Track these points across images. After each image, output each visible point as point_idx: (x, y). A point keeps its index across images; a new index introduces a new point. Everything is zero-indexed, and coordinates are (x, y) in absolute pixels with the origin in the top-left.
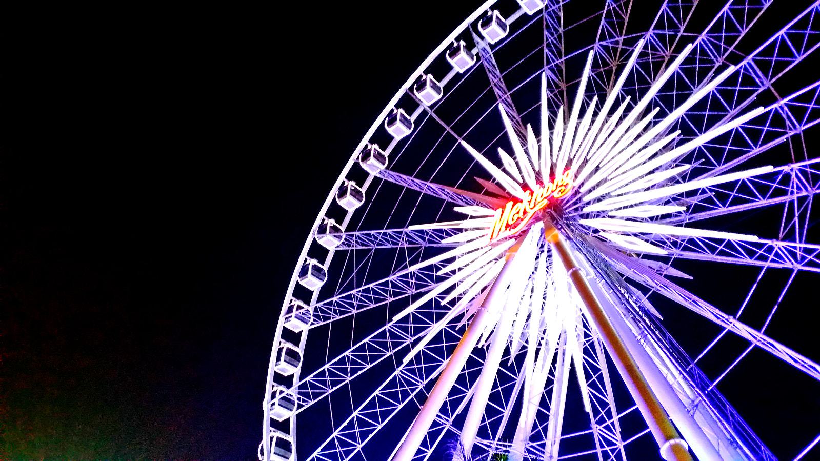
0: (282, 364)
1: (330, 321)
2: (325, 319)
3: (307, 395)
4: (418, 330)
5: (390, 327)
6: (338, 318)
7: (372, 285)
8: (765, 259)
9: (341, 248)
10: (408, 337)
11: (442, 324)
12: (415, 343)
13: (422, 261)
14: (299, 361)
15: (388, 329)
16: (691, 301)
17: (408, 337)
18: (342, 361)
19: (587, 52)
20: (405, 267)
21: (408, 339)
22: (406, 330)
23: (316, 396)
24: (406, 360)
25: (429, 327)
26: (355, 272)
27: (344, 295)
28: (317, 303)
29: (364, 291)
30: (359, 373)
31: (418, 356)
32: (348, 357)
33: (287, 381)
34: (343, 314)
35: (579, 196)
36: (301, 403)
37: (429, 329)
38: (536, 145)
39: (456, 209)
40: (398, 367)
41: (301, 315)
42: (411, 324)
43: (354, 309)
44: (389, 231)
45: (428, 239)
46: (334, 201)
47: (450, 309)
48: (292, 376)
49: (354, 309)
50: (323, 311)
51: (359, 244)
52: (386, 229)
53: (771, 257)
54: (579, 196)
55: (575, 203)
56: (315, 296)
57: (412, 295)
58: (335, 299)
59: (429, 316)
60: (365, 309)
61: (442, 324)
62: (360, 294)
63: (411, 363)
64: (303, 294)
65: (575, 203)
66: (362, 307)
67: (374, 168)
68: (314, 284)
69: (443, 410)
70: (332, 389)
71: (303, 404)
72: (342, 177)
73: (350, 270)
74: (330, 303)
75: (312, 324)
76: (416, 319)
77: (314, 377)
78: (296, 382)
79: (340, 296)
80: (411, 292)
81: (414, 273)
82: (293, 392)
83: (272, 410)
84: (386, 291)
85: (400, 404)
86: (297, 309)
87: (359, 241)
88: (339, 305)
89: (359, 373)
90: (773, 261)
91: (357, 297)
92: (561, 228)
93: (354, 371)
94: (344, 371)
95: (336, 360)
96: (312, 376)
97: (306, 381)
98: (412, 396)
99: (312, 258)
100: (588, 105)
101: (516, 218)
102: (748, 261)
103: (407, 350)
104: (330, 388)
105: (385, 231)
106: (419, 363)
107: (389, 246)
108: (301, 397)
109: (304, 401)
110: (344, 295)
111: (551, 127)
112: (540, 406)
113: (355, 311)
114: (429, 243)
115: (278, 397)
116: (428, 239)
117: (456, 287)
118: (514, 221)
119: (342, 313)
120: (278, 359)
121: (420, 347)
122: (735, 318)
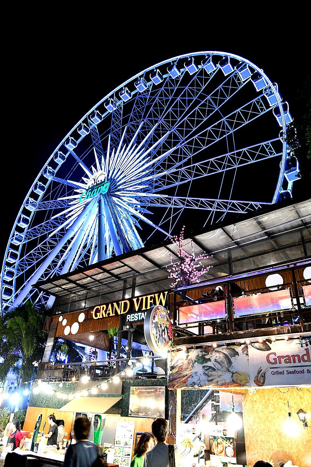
1: (48, 253)
10: (183, 171)
11: (165, 173)
12: (180, 167)
13: (148, 133)
19: (125, 126)
24: (186, 160)
25: (170, 173)
26: (172, 216)
30: (219, 157)
31: (181, 160)
35: (116, 186)
38: (90, 232)
42: (226, 162)
54: (116, 186)
55: (115, 186)
61: (165, 173)
63: (185, 158)
65: (115, 186)
73: (174, 219)
77: (248, 162)
84: (46, 247)
92: (187, 325)
98: (235, 152)
100: (123, 146)
103: (185, 164)
104: (227, 156)
106: (181, 157)
111: (100, 164)
121: (178, 164)
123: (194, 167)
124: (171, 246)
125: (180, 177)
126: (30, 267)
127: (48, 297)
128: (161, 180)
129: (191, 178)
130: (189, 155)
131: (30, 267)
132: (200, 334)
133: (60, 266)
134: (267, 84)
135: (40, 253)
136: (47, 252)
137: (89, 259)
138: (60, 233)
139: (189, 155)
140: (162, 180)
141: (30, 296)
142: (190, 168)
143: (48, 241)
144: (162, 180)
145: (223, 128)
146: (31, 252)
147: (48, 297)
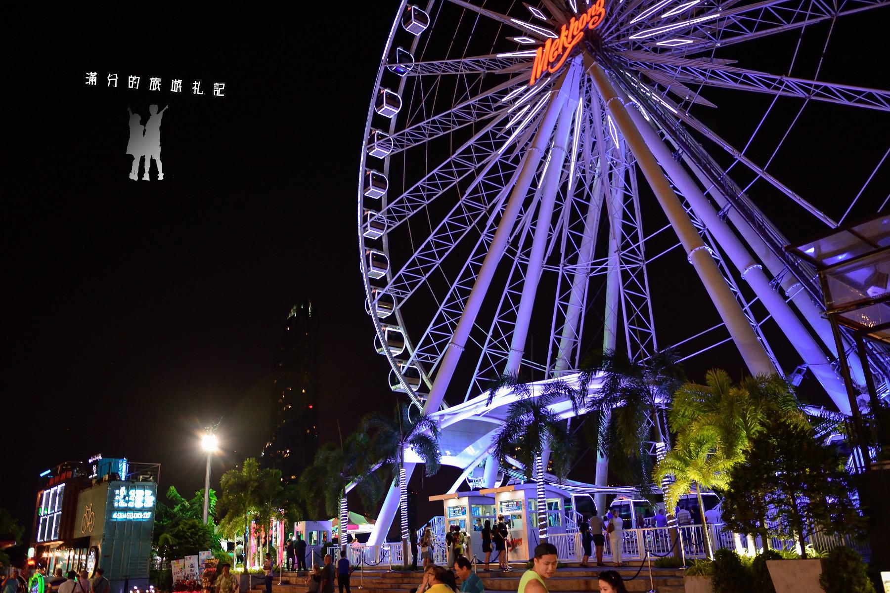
0: (373, 270)
1: (406, 218)
2: (400, 218)
4: (491, 197)
10: (482, 207)
15: (464, 204)
16: (741, 79)
17: (482, 207)
18: (428, 247)
21: (484, 209)
23: (412, 286)
27: (414, 127)
28: (388, 205)
29: (428, 179)
30: (446, 254)
32: (432, 240)
33: (382, 283)
40: (482, 232)
42: (482, 192)
43: (425, 200)
44: (436, 117)
45: (476, 113)
46: (375, 113)
47: (515, 168)
48: (385, 277)
49: (425, 200)
50: (396, 211)
52: (433, 117)
57: (476, 170)
58: (407, 130)
59: (498, 180)
60: (434, 197)
62: (426, 183)
64: (381, 122)
66: (433, 135)
67: (406, 70)
68: (391, 112)
70: (425, 275)
72: (377, 86)
75: (389, 227)
76: (487, 187)
77: (434, 325)
79: (411, 128)
80: (473, 120)
82: (389, 289)
83: (377, 312)
84: (403, 207)
85: (497, 321)
86: (378, 139)
91: (428, 129)
93: (441, 254)
94: (432, 256)
95: (423, 246)
96: (404, 268)
99: (377, 128)
105: (433, 119)
107: (442, 134)
110: (414, 127)
112: (623, 219)
113: (427, 140)
115: (377, 298)
116: (476, 113)
117: (523, 205)
118: (555, 58)
119: (414, 208)
122: (787, 76)
123: (471, 223)
124: (823, 378)
126: (415, 211)
127: (731, 338)
129: (464, 202)
130: (466, 201)
131: (415, 211)
133: (492, 226)
134: (368, 257)
135: (436, 186)
137: (393, 370)
139: (466, 201)
142: (475, 217)
146: (419, 184)
147: (731, 338)
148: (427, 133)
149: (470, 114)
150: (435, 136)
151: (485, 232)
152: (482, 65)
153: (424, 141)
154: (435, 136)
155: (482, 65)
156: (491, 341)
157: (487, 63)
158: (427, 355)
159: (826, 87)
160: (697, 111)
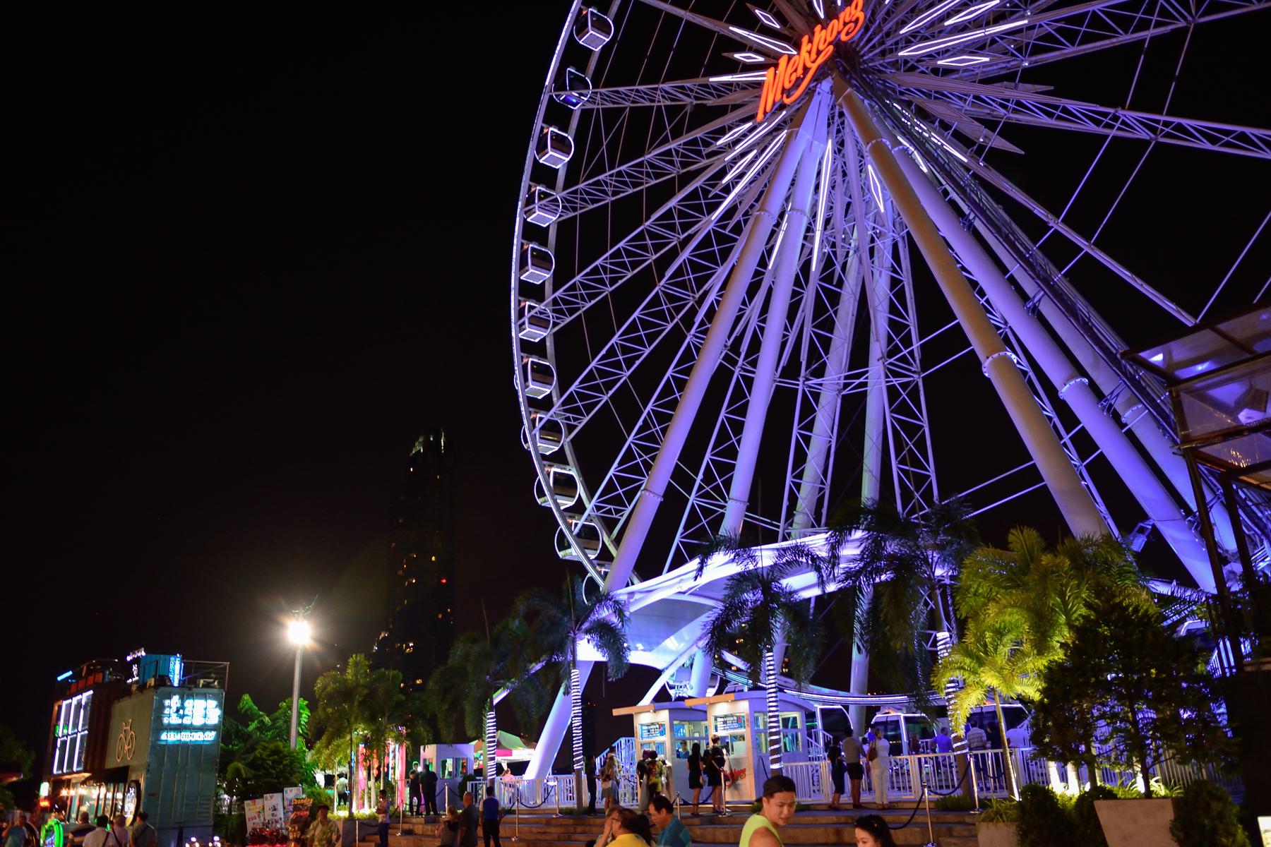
0: (532, 386)
2: (572, 312)
3: (576, 411)
4: (701, 282)
5: (663, 286)
6: (588, 305)
7: (621, 245)
8: (1111, 127)
9: (565, 217)
10: (689, 296)
13: (680, 189)
14: (553, 376)
15: (662, 291)
17: (689, 296)
18: (612, 352)
20: (665, 141)
22: (682, 285)
23: (589, 408)
27: (591, 181)
29: (612, 256)
30: (638, 363)
32: (617, 343)
33: (546, 404)
34: (594, 299)
36: (573, 423)
37: (716, 275)
39: (691, 753)
41: (539, 315)
45: (681, 162)
47: (736, 240)
50: (565, 302)
51: (587, 202)
53: (1118, 125)
56: (548, 288)
57: (680, 242)
58: (581, 186)
59: (711, 257)
62: (614, 178)
66: (618, 193)
69: (749, 382)
70: (607, 393)
71: (575, 423)
74: (573, 287)
75: (555, 324)
76: (696, 267)
78: (557, 402)
79: (587, 183)
81: (675, 208)
82: (556, 412)
83: (538, 445)
84: (575, 296)
87: (586, 197)
88: (585, 286)
89: (638, 363)
90: (1119, 129)
91: (611, 184)
93: (629, 363)
94: (617, 365)
95: (604, 352)
97: (572, 392)
101: (794, 77)
102: (1091, 127)
107: (631, 191)
108: (571, 415)
109: (575, 419)
110: (591, 181)
113: (609, 199)
114: (683, 168)
115: (538, 425)
118: (792, 83)
119: (591, 297)
120: (526, 380)
123: (672, 318)
125: (654, 430)
126: (593, 302)
127: (764, 270)
128: (716, 196)
129: (663, 289)
131: (593, 302)
132: (214, 730)
135: (623, 265)
136: (579, 309)
137: (561, 529)
138: (611, 264)
140: (712, 198)
141: (654, 257)
142: (678, 310)
143: (648, 230)
144: (711, 198)
145: (716, 489)
147: (764, 270)
148: (609, 190)
149: (672, 163)
150: (622, 195)
151: (693, 331)
152: (645, 96)
153: (606, 202)
154: (622, 195)
155: (645, 96)
156: (700, 488)
157: (695, 90)
158: (609, 507)
159: (1179, 125)
160: (996, 159)
